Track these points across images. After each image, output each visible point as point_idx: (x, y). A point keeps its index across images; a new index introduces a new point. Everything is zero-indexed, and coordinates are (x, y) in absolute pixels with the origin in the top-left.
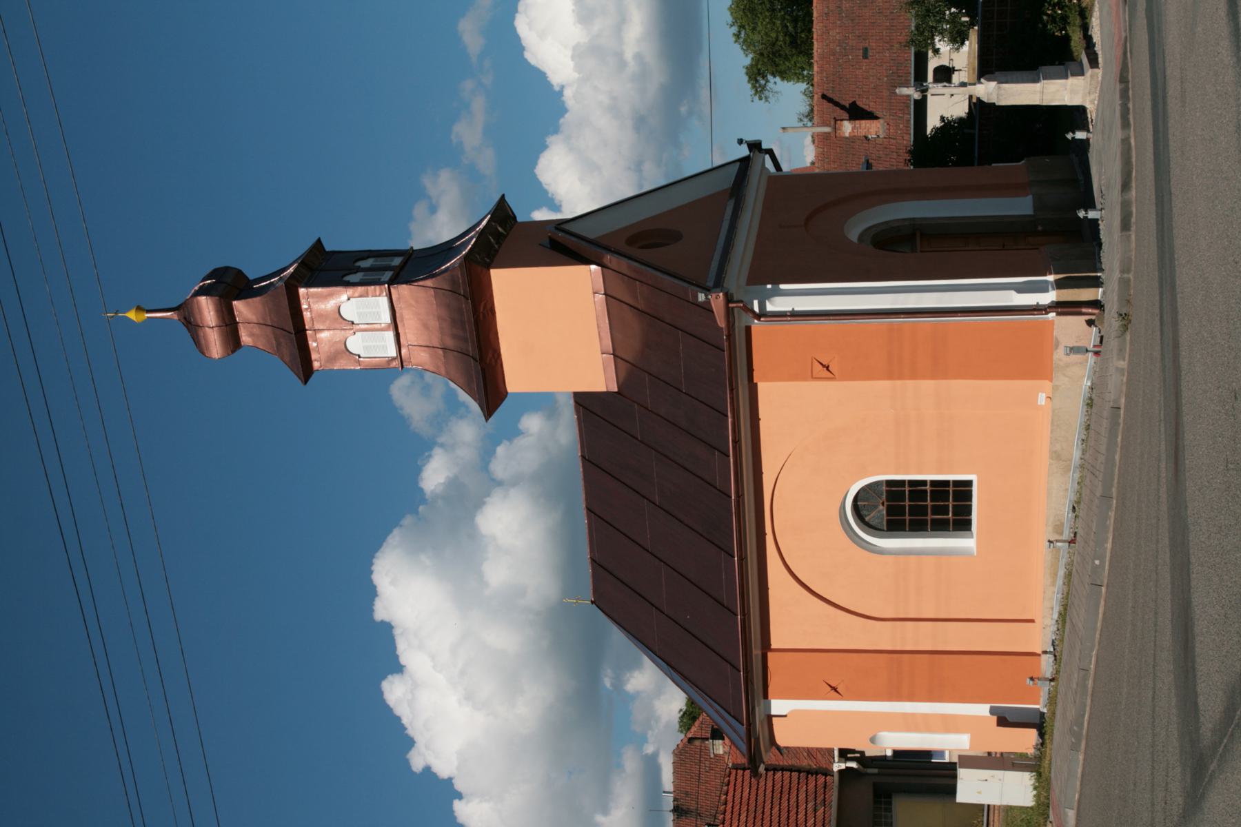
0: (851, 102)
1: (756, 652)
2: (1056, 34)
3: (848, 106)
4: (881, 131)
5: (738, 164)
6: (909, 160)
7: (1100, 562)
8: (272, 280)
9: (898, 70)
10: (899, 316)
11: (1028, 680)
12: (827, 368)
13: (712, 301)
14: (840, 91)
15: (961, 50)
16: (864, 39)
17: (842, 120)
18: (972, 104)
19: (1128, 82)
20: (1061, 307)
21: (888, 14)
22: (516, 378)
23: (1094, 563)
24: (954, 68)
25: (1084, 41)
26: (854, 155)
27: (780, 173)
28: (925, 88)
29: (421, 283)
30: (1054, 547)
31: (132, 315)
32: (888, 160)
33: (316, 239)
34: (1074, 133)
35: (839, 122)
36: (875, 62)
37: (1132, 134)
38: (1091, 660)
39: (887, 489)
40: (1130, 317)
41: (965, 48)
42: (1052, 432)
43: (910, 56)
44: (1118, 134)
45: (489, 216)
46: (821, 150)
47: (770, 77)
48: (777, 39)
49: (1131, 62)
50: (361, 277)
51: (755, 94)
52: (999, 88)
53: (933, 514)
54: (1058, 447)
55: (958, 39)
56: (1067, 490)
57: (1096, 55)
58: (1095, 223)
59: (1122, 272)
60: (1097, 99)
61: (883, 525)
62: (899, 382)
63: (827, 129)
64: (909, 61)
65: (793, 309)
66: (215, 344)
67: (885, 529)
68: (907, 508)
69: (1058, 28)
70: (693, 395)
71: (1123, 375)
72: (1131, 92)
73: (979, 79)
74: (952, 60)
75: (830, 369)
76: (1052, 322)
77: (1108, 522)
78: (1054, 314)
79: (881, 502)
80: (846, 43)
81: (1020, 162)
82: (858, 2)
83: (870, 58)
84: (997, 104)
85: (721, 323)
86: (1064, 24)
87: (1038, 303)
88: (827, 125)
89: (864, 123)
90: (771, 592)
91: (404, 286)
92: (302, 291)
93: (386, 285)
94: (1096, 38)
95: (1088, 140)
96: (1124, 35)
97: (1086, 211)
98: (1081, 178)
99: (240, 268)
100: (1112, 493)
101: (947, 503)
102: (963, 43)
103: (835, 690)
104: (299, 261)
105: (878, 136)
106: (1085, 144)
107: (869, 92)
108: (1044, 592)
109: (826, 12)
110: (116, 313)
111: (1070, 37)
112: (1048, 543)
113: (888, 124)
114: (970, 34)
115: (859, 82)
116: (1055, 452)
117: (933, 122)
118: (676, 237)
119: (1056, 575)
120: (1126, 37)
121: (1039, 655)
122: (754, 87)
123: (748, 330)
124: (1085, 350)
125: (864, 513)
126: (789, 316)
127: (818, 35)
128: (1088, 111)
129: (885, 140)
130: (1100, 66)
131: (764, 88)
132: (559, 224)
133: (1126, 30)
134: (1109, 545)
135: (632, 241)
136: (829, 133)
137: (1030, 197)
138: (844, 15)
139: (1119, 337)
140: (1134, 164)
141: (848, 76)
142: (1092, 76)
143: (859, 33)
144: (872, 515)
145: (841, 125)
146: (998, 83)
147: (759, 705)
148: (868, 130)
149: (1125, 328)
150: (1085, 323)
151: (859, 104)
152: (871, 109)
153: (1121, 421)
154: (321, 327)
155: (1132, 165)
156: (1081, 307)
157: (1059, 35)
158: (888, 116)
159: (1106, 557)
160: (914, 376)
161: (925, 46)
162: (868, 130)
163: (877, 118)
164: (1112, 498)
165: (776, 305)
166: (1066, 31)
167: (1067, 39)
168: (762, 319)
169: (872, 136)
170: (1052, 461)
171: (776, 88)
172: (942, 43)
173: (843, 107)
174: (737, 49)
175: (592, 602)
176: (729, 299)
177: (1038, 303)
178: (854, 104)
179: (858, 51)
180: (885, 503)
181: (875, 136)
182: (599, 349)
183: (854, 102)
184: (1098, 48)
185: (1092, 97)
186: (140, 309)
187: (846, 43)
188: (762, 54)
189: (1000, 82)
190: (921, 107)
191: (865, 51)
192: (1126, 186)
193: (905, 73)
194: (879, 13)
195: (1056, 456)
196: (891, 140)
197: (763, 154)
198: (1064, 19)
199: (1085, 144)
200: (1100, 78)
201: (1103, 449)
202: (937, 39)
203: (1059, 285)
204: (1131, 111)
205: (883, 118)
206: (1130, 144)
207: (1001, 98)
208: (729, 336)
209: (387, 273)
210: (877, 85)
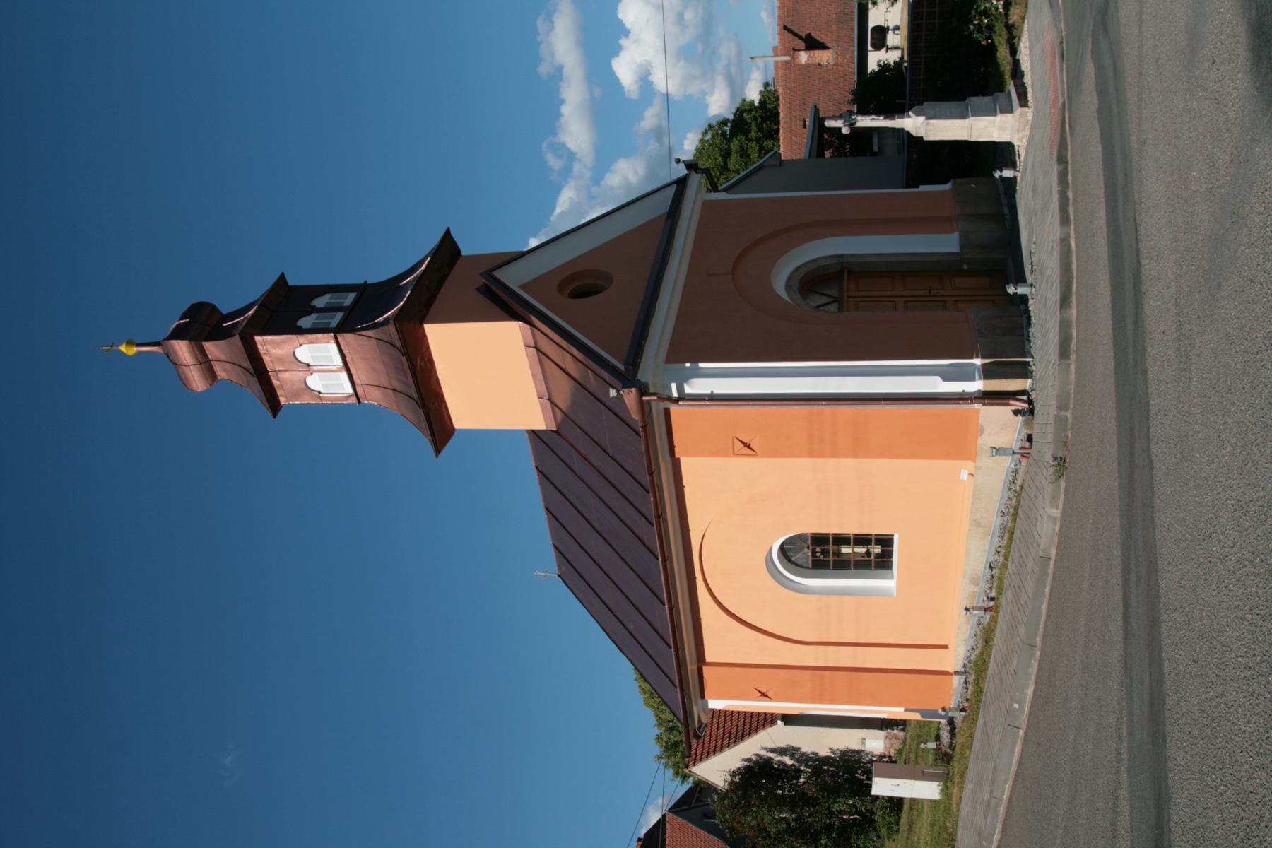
1: (691, 667)
2: (983, 43)
3: (804, 36)
5: (675, 186)
7: (1019, 707)
8: (238, 320)
10: (821, 403)
13: (624, 397)
17: (799, 50)
19: (1067, 162)
20: (988, 399)
22: (462, 415)
24: (888, 27)
28: (853, 121)
29: (363, 333)
31: (123, 348)
32: (837, 83)
33: (280, 273)
34: (1001, 171)
35: (796, 52)
37: (1072, 233)
38: (1004, 792)
40: (1066, 464)
42: (973, 503)
45: (429, 259)
50: (313, 321)
57: (1025, 88)
59: (1060, 408)
62: (820, 460)
63: (787, 58)
66: (197, 381)
67: (810, 566)
69: (984, 37)
71: (1055, 524)
72: (1070, 178)
74: (887, 20)
75: (751, 446)
76: (978, 411)
77: (1030, 669)
79: (806, 546)
81: (944, 182)
84: (925, 139)
86: (991, 33)
90: (703, 622)
91: (349, 335)
92: (258, 339)
94: (1025, 65)
95: (1015, 178)
96: (1061, 100)
98: (1006, 211)
99: (214, 303)
100: (1036, 642)
104: (259, 303)
105: (829, 64)
108: (958, 628)
110: (111, 346)
112: (965, 612)
113: (837, 54)
116: (975, 520)
117: (872, 66)
120: (1064, 103)
121: (951, 674)
123: (667, 411)
124: (1012, 452)
125: (791, 554)
126: (709, 400)
129: (834, 67)
130: (1029, 104)
133: (1064, 93)
136: (789, 61)
139: (1054, 483)
142: (1021, 115)
145: (799, 55)
146: (927, 119)
147: (696, 704)
150: (1011, 412)
151: (814, 35)
153: (1050, 571)
154: (281, 369)
155: (1072, 273)
156: (1009, 399)
159: (1026, 702)
160: (834, 455)
164: (1036, 647)
165: (696, 387)
166: (992, 40)
167: (992, 48)
168: (680, 403)
169: (824, 62)
173: (800, 37)
175: (559, 576)
178: (809, 36)
180: (810, 547)
184: (1028, 79)
185: (1021, 135)
189: (929, 118)
192: (1065, 301)
195: (975, 523)
198: (990, 28)
203: (988, 373)
204: (1071, 202)
206: (1069, 245)
208: (644, 427)
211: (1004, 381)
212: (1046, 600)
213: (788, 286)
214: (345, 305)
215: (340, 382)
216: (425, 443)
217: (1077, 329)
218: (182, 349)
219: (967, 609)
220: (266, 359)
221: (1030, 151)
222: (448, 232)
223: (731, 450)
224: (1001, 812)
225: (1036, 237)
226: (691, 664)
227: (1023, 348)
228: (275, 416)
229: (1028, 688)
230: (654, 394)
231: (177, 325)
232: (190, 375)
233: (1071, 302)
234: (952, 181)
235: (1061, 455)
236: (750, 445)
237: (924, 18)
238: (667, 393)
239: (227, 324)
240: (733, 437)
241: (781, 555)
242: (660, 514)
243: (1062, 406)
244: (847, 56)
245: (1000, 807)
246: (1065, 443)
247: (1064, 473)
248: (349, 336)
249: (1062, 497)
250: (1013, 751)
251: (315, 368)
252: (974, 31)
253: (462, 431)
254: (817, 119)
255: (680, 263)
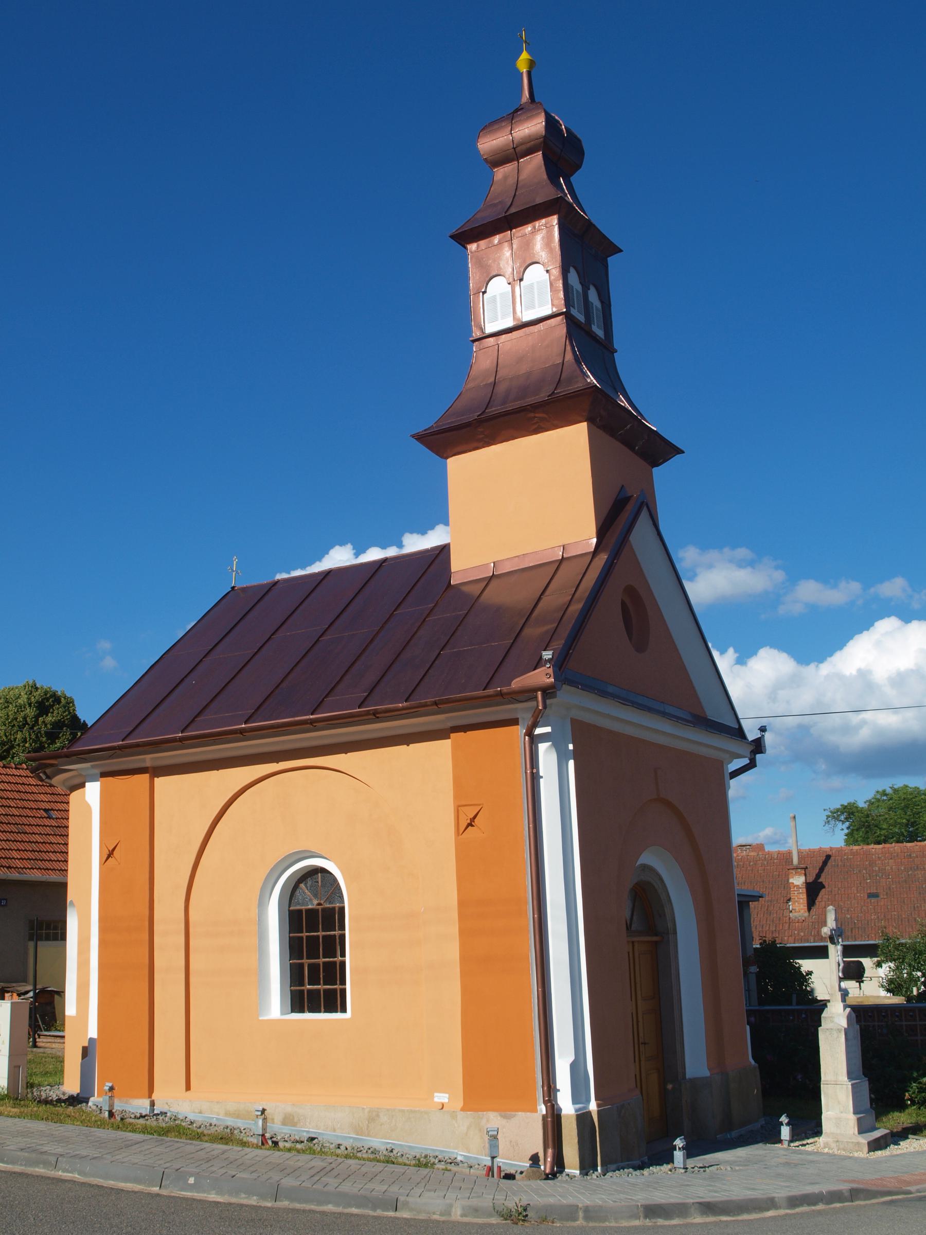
0: (824, 883)
1: (148, 760)
2: (907, 1094)
3: (820, 880)
4: (796, 914)
5: (737, 727)
6: (765, 941)
8: (568, 195)
9: (858, 928)
10: (536, 912)
11: (110, 1084)
12: (470, 825)
13: (543, 668)
14: (835, 873)
15: (881, 989)
16: (887, 893)
17: (805, 875)
18: (825, 1002)
20: (553, 1122)
21: (913, 916)
23: (191, 1175)
24: (862, 982)
25: (900, 1129)
26: (772, 888)
27: (727, 776)
29: (569, 348)
30: (257, 1116)
31: (523, 61)
32: (768, 922)
34: (788, 1124)
35: (804, 872)
36: (865, 906)
37: (782, 1212)
38: (67, 1171)
39: (337, 909)
40: (521, 1223)
41: (883, 993)
42: (403, 1111)
43: (872, 940)
44: (781, 1191)
46: (776, 857)
47: (847, 824)
48: (881, 829)
49: (878, 1203)
51: (831, 812)
52: (839, 1031)
53: (309, 965)
54: (384, 1118)
55: (893, 986)
56: (334, 1130)
58: (670, 1159)
59: (587, 1210)
60: (831, 1152)
61: (295, 906)
62: (455, 915)
63: (795, 861)
64: (867, 939)
65: (542, 777)
66: (489, 143)
68: (315, 934)
70: (436, 662)
71: (441, 1214)
72: (838, 1205)
73: (849, 1006)
76: (534, 1110)
77: (243, 1195)
78: (544, 1112)
79: (322, 902)
80: (882, 876)
81: (754, 1058)
82: (924, 886)
83: (869, 900)
84: (820, 1029)
85: (517, 683)
87: (559, 1090)
88: (800, 862)
89: (804, 897)
91: (565, 330)
92: (554, 220)
93: (565, 310)
96: (913, 1188)
97: (683, 1148)
98: (735, 1134)
101: (322, 982)
102: (888, 991)
103: (109, 856)
106: (775, 1138)
107: (835, 900)
109: (912, 855)
110: (526, 42)
111: (904, 1111)
112: (261, 1109)
114: (898, 997)
115: (845, 891)
116: (378, 1116)
117: (806, 965)
118: (641, 647)
119: (238, 1117)
120: (910, 1192)
121: (150, 1096)
122: (838, 810)
123: (514, 722)
125: (309, 882)
126: (532, 773)
127: (888, 848)
128: (816, 1139)
129: (787, 918)
131: (837, 819)
132: (647, 505)
133: (920, 1192)
134: (213, 1197)
135: (631, 591)
137: (707, 1073)
138: (910, 873)
139: (494, 1209)
140: (740, 1218)
141: (849, 879)
143: (893, 888)
144: (306, 891)
146: (845, 1029)
147: (93, 767)
148: (797, 901)
149: (507, 1215)
150: (535, 1152)
151: (823, 892)
152: (817, 903)
153: (379, 1212)
154: (515, 246)
155: (738, 1214)
156: (554, 1148)
157: (906, 1098)
158: (811, 921)
159: (198, 1193)
160: (463, 933)
161: (883, 953)
162: (797, 901)
163: (809, 909)
165: (546, 754)
166: (910, 1105)
170: (366, 1111)
171: (837, 830)
172: (888, 969)
173: (818, 876)
174: (870, 795)
175: (233, 588)
176: (548, 692)
177: (559, 1090)
178: (822, 886)
179: (875, 888)
180: (320, 907)
181: (791, 909)
182: (496, 560)
183: (823, 887)
184: (893, 1150)
185: (833, 1145)
186: (532, 64)
187: (882, 876)
188: (868, 816)
190: (821, 953)
191: (875, 895)
192: (708, 1208)
193: (855, 936)
194: (914, 907)
196: (788, 924)
197: (749, 756)
199: (775, 1138)
200: (856, 1155)
201: (346, 1187)
202: (892, 965)
203: (583, 1119)
204: (813, 1208)
205: (809, 915)
206: (768, 1209)
207: (828, 1033)
208: (501, 694)
209: (583, 317)
210: (842, 909)
211: (576, 1140)
212: (340, 1209)
213: (646, 868)
214: (593, 326)
215: (499, 317)
216: (427, 421)
217: (679, 1225)
218: (534, 126)
219: (263, 1111)
220: (528, 228)
221: (825, 1157)
222: (679, 451)
223: (464, 803)
224: (37, 1169)
225: (740, 1170)
226: (152, 759)
227: (611, 1162)
228: (452, 237)
229: (217, 1194)
230: (545, 707)
231: (558, 122)
232: (499, 134)
233: (708, 1216)
234: (757, 1065)
235: (530, 1215)
236: (472, 826)
237: (921, 1023)
238: (542, 721)
239: (562, 182)
240: (483, 804)
241: (315, 868)
242: (377, 716)
243: (590, 1214)
244: (802, 934)
245: (44, 1168)
246: (544, 1220)
247: (509, 1221)
248: (563, 330)
249: (480, 1221)
250: (126, 1180)
251: (517, 289)
252: (920, 1083)
253: (651, 475)
254: (747, 899)
255: (664, 733)
